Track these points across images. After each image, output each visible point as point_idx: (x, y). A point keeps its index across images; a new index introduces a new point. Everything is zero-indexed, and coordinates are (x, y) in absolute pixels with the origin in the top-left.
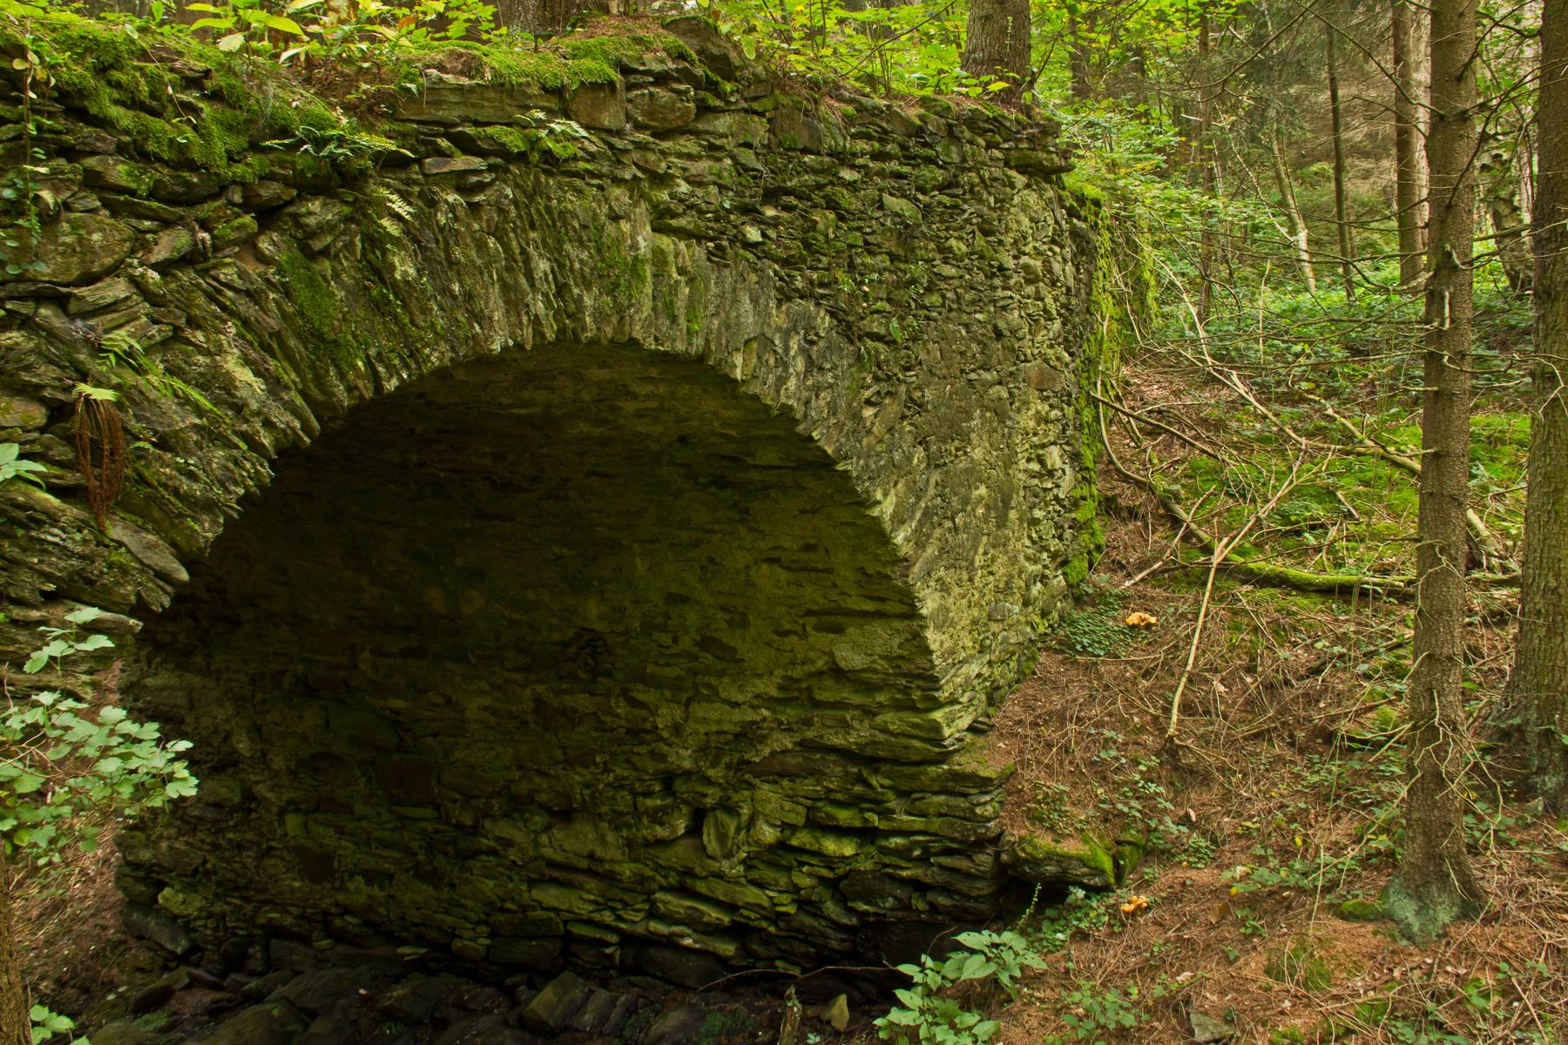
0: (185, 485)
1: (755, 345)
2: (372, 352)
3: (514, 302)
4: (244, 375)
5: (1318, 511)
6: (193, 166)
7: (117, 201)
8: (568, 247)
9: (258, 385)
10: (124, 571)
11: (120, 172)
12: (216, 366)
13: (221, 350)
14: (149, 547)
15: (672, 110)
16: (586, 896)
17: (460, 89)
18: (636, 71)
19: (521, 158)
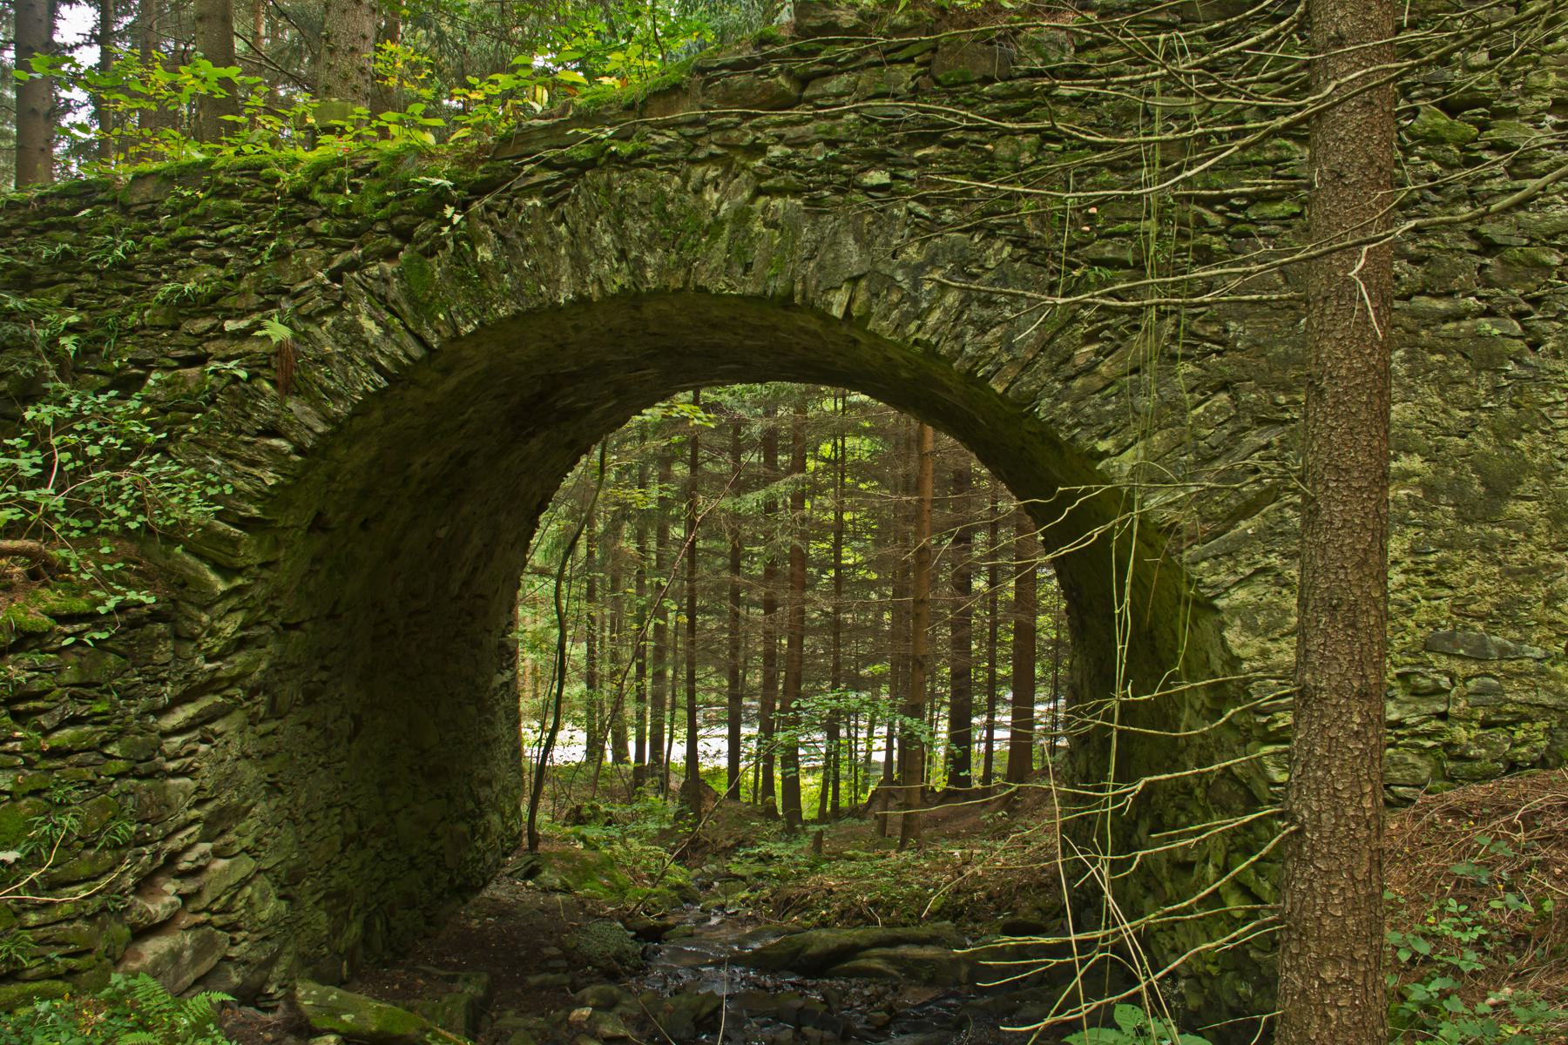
0: (327, 383)
1: (863, 283)
2: (453, 308)
3: (579, 264)
4: (369, 325)
5: (99, 332)
6: (354, 216)
7: (321, 240)
8: (628, 222)
9: (377, 331)
10: (292, 424)
11: (322, 226)
12: (355, 321)
13: (358, 312)
14: (306, 413)
15: (751, 89)
16: (1417, 479)
17: (546, 127)
18: (712, 69)
19: (591, 164)
